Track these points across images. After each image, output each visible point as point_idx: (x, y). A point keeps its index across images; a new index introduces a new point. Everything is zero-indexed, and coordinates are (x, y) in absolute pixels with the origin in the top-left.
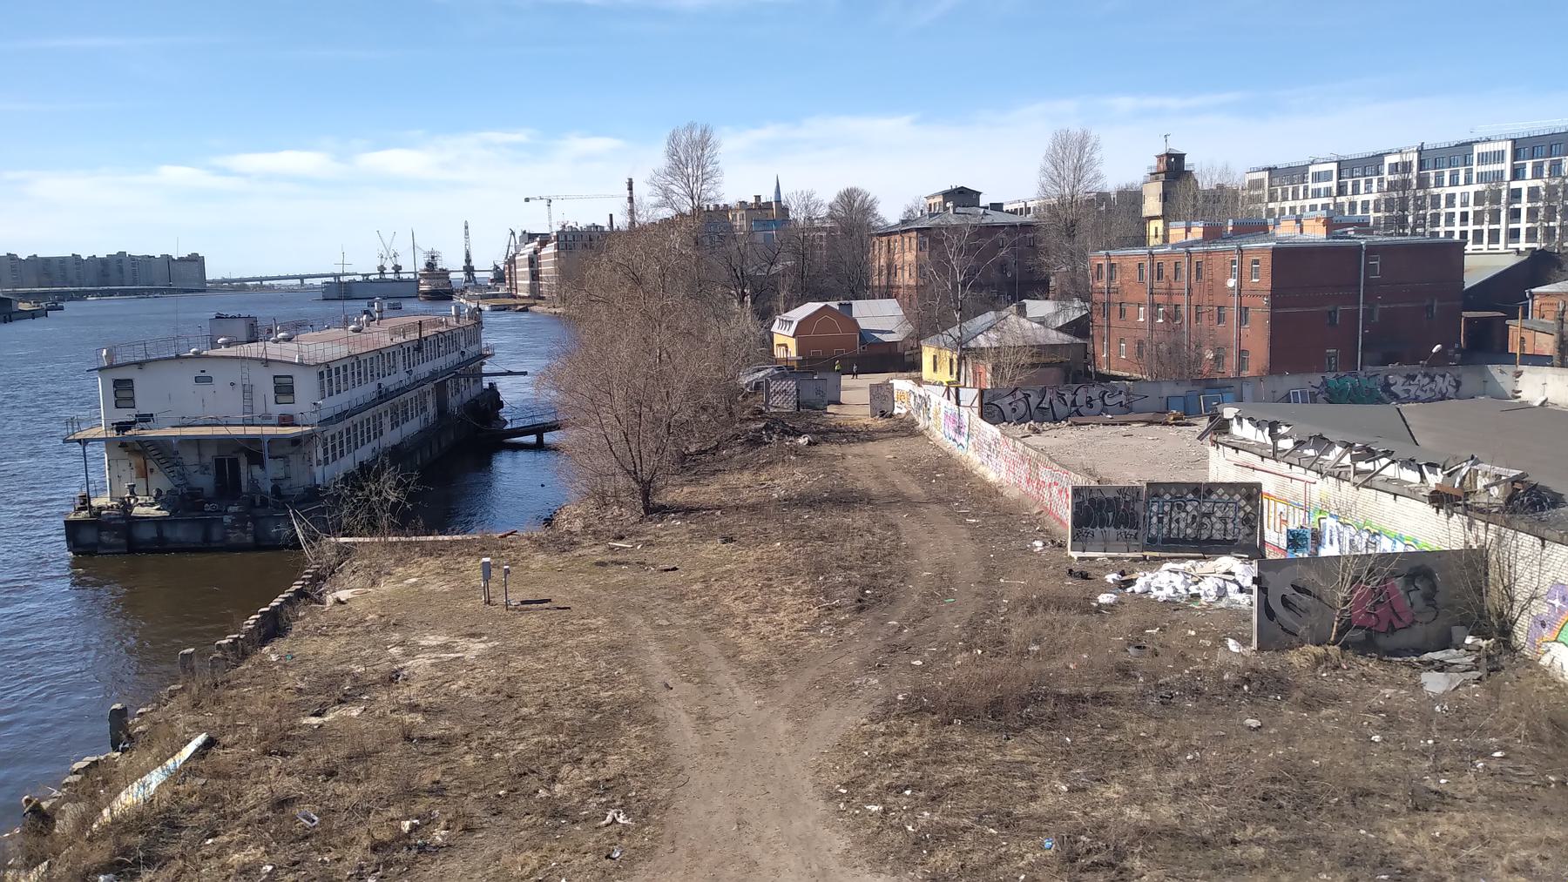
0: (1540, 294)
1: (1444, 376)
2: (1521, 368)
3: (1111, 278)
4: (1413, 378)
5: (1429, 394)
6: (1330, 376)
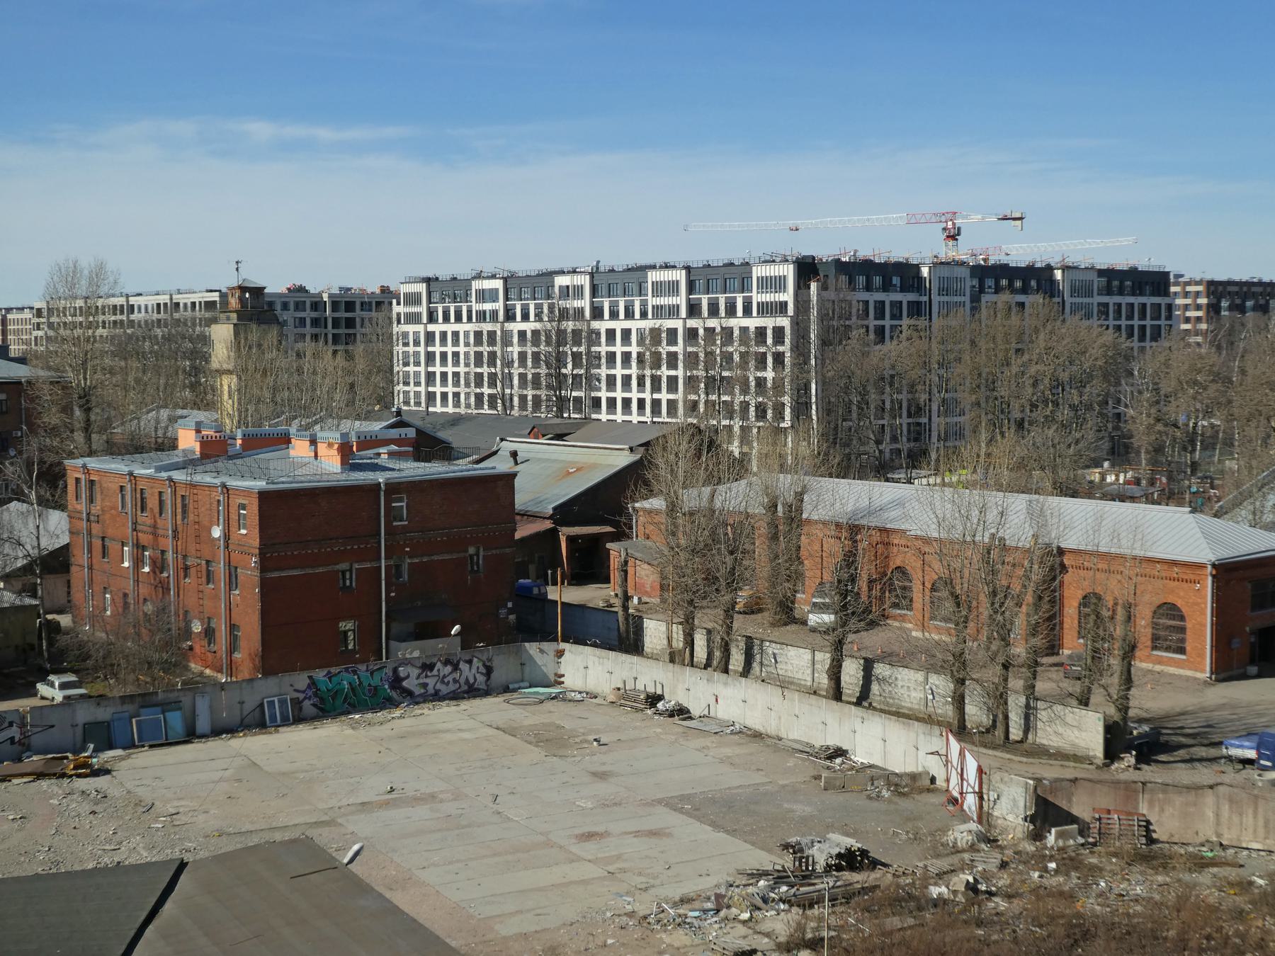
0: (644, 510)
1: (470, 662)
2: (563, 645)
3: (91, 500)
4: (431, 667)
5: (452, 687)
6: (320, 675)
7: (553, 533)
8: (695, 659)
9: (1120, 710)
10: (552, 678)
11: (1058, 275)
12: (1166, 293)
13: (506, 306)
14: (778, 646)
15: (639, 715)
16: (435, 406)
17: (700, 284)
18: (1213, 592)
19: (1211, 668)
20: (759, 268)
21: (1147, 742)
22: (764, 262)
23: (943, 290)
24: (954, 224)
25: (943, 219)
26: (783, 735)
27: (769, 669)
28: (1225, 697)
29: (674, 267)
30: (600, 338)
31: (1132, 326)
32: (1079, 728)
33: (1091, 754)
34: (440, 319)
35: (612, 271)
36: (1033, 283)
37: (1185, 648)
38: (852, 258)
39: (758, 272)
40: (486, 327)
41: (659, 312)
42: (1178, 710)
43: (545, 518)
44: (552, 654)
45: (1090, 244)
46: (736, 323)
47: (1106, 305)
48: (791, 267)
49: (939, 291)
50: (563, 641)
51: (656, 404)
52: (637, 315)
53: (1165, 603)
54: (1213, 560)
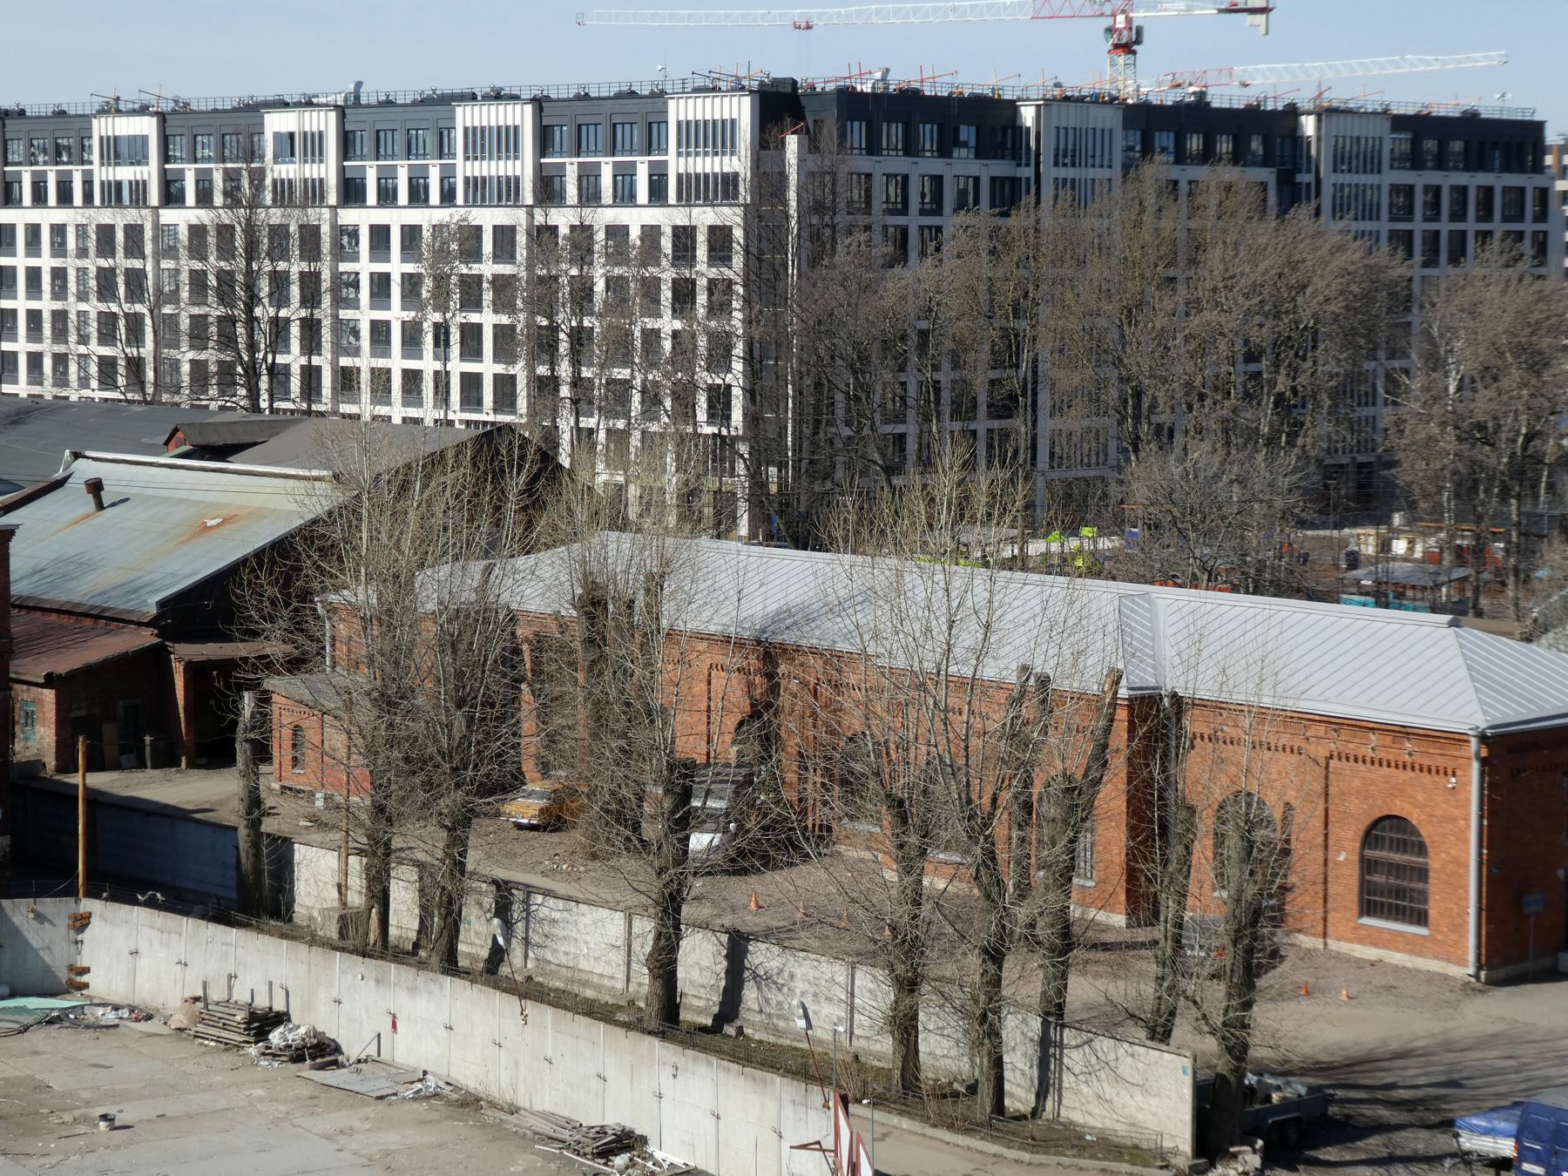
2: (88, 905)
7: (155, 658)
8: (393, 931)
9: (1229, 1050)
10: (63, 975)
11: (1309, 125)
12: (1538, 168)
13: (163, 173)
14: (561, 904)
15: (230, 1058)
16: (16, 382)
17: (366, 142)
18: (1481, 795)
19: (1479, 955)
20: (682, 102)
21: (1297, 1119)
22: (696, 90)
23: (1065, 156)
24: (1129, 20)
25: (1107, 9)
26: (522, 1102)
27: (541, 952)
28: (1501, 1019)
29: (514, 98)
30: (357, 243)
31: (1437, 233)
32: (1143, 1088)
33: (1167, 1144)
34: (27, 199)
35: (389, 103)
36: (1256, 145)
37: (1426, 913)
38: (881, 85)
39: (679, 111)
40: (119, 218)
41: (479, 191)
42: (1394, 1046)
43: (140, 624)
44: (63, 922)
45: (1412, 65)
46: (604, 217)
47: (1409, 190)
48: (746, 102)
49: (1056, 156)
50: (89, 894)
51: (471, 383)
52: (435, 197)
53: (1388, 817)
54: (1483, 725)
